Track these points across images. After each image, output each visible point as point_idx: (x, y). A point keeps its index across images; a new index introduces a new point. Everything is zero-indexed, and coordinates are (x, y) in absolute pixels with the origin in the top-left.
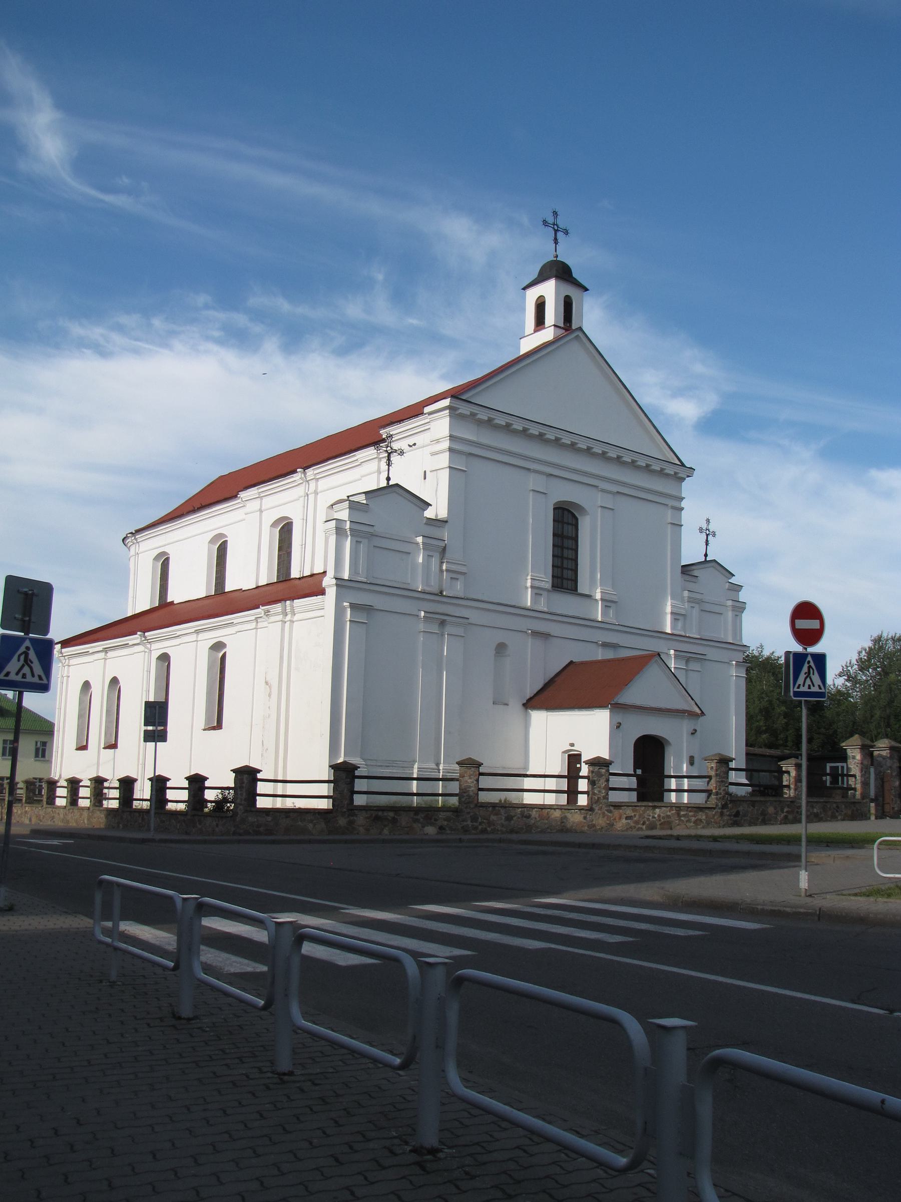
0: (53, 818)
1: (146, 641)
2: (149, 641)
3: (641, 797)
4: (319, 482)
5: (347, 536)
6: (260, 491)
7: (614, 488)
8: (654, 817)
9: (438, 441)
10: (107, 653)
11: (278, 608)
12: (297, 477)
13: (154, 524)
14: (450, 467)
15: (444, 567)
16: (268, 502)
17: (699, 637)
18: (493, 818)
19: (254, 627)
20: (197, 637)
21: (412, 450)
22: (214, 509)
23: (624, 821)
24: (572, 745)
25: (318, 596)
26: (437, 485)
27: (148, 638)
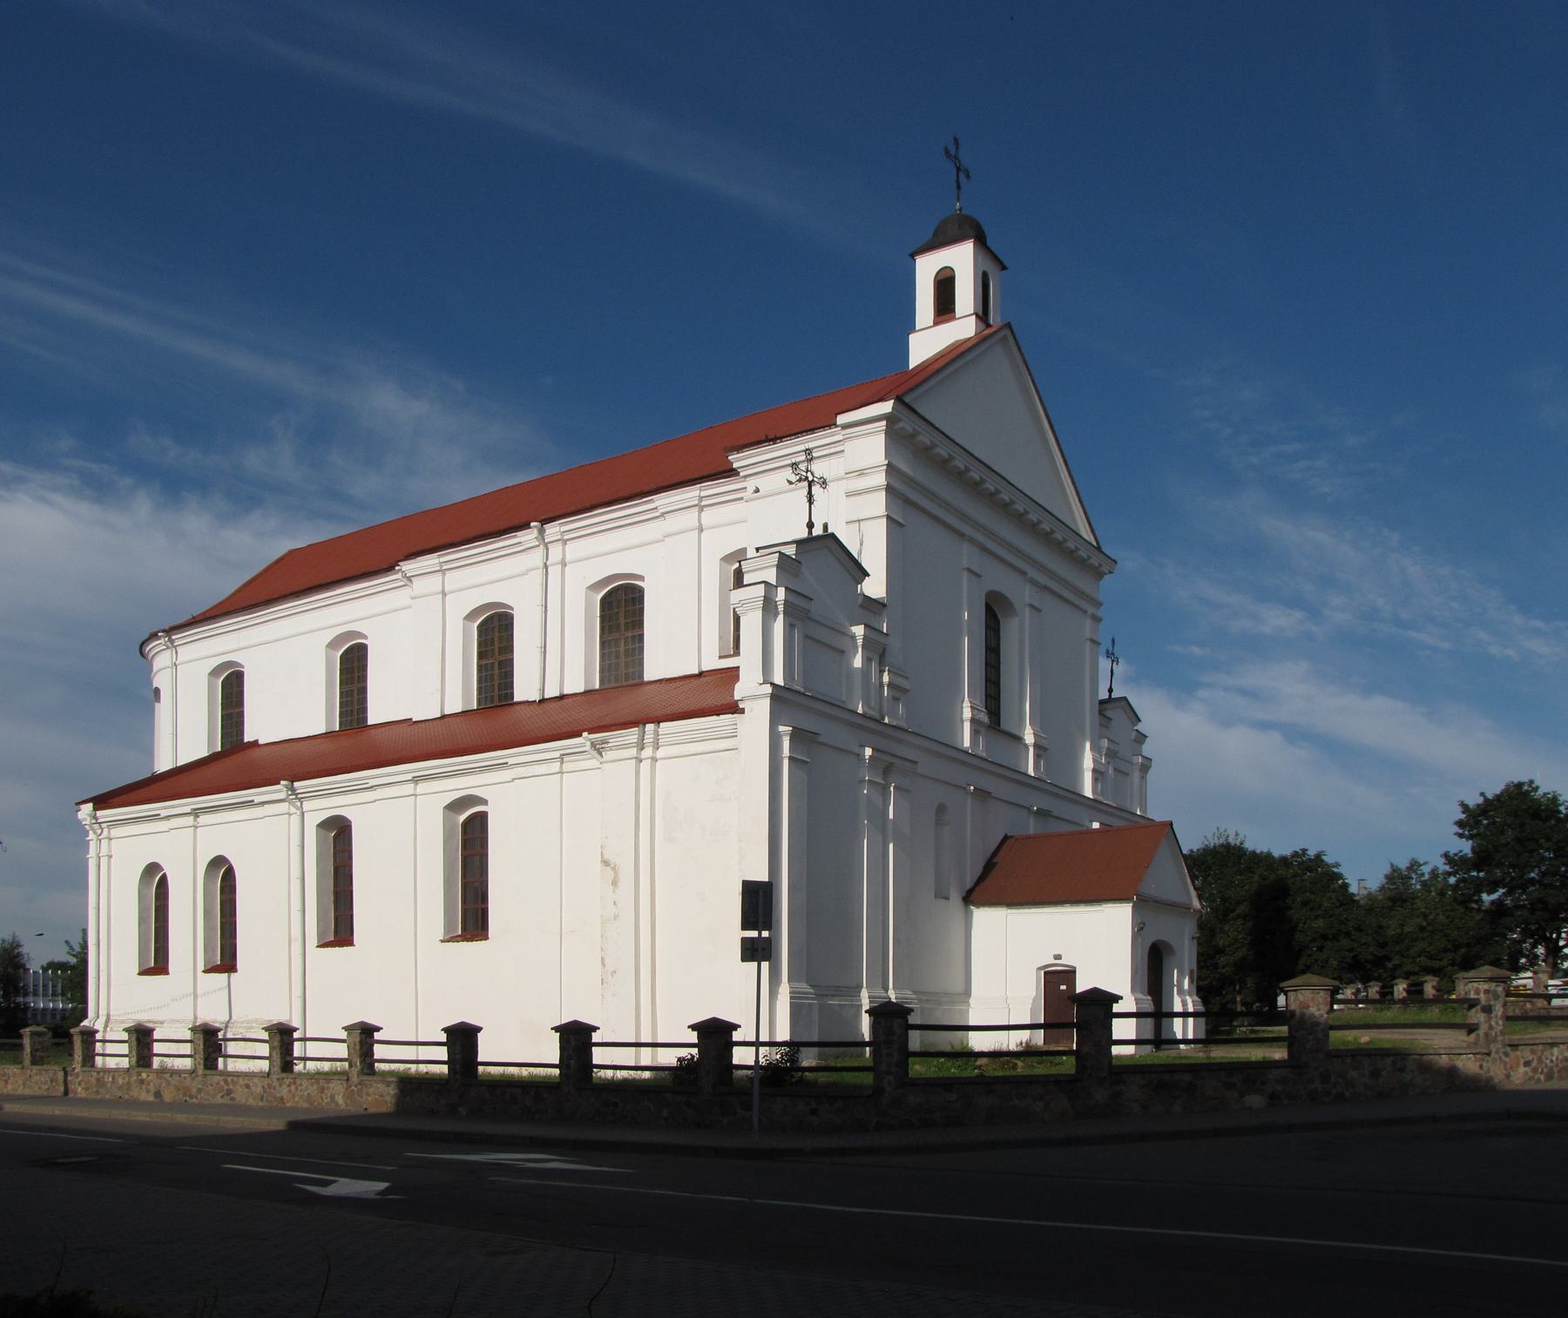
0: (229, 1092)
1: (294, 797)
2: (299, 796)
3: (149, 1032)
4: (567, 546)
5: (776, 615)
6: (442, 560)
7: (1042, 579)
8: (1552, 1061)
9: (861, 473)
10: (198, 817)
11: (631, 735)
12: (528, 537)
13: (207, 615)
14: (888, 517)
15: (886, 678)
16: (454, 579)
17: (1115, 805)
18: (1353, 1074)
19: (558, 770)
20: (415, 789)
21: (795, 490)
22: (339, 591)
23: (1522, 1069)
24: (1058, 957)
25: (721, 716)
26: (861, 544)
27: (298, 791)
